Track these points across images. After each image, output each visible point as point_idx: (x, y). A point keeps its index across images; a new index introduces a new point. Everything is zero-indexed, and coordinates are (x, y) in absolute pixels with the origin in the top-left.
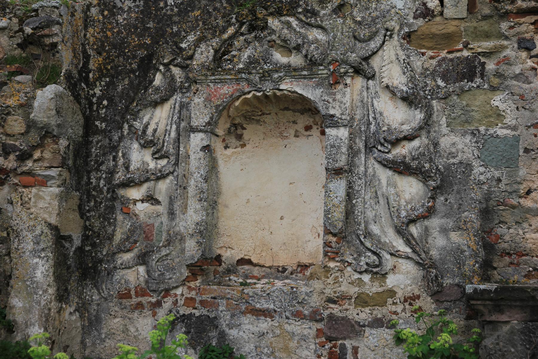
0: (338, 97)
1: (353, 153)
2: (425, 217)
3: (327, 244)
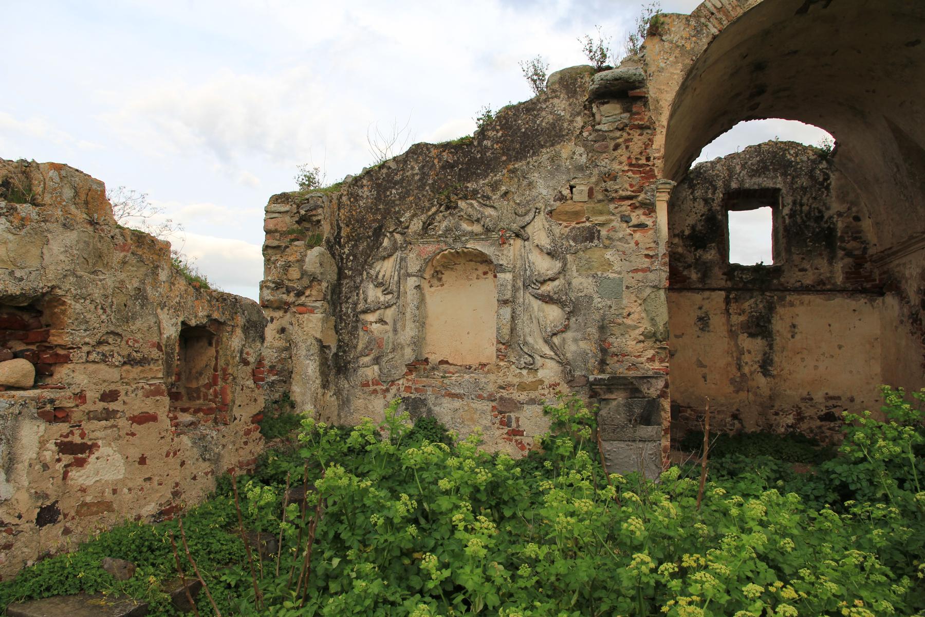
0: (505, 252)
1: (515, 289)
2: (562, 332)
3: (498, 350)
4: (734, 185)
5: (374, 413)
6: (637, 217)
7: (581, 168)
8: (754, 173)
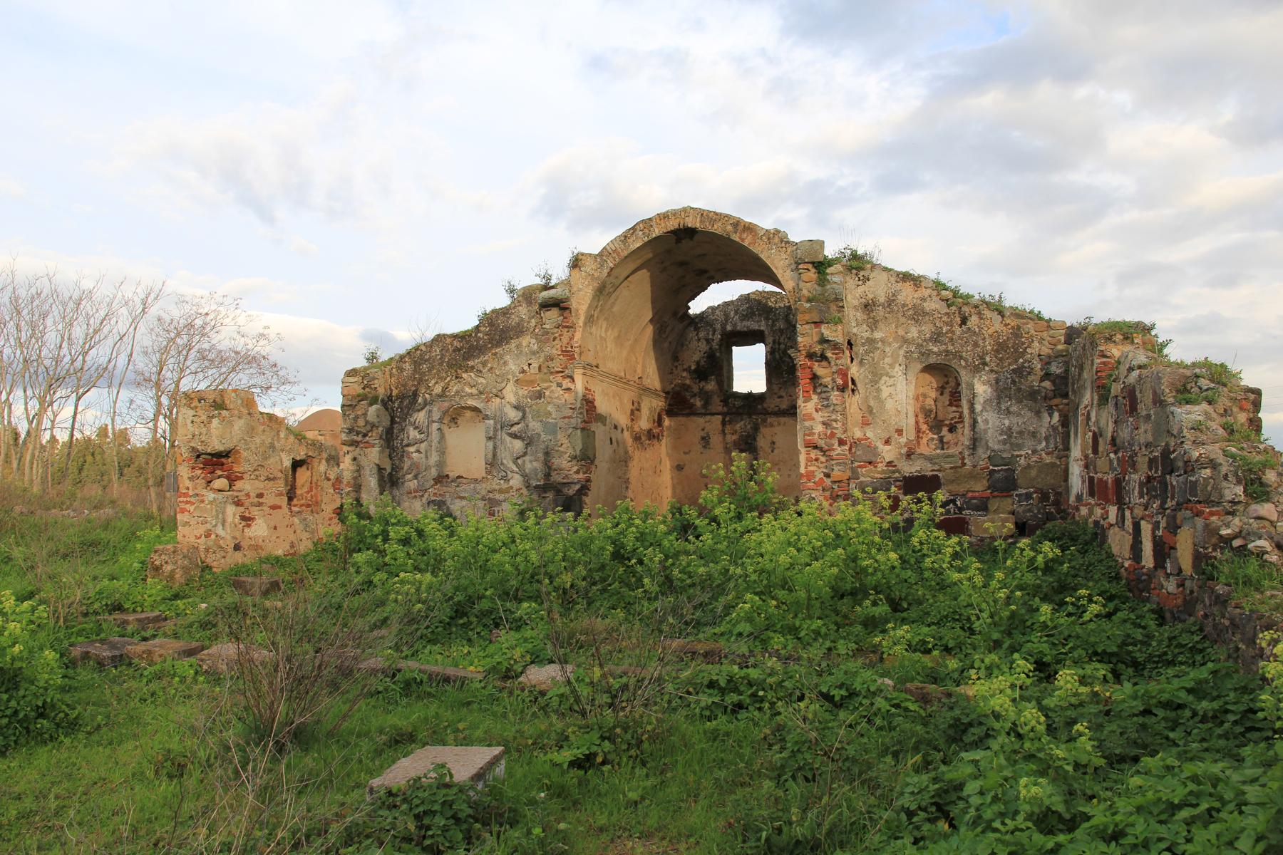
1: (496, 430)
4: (729, 328)
5: (415, 509)
6: (567, 383)
7: (534, 353)
8: (745, 317)
